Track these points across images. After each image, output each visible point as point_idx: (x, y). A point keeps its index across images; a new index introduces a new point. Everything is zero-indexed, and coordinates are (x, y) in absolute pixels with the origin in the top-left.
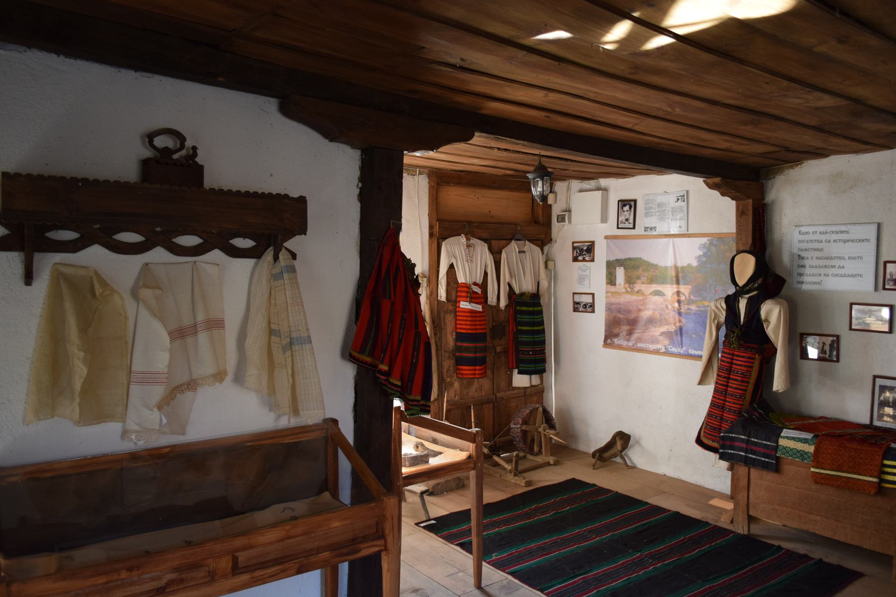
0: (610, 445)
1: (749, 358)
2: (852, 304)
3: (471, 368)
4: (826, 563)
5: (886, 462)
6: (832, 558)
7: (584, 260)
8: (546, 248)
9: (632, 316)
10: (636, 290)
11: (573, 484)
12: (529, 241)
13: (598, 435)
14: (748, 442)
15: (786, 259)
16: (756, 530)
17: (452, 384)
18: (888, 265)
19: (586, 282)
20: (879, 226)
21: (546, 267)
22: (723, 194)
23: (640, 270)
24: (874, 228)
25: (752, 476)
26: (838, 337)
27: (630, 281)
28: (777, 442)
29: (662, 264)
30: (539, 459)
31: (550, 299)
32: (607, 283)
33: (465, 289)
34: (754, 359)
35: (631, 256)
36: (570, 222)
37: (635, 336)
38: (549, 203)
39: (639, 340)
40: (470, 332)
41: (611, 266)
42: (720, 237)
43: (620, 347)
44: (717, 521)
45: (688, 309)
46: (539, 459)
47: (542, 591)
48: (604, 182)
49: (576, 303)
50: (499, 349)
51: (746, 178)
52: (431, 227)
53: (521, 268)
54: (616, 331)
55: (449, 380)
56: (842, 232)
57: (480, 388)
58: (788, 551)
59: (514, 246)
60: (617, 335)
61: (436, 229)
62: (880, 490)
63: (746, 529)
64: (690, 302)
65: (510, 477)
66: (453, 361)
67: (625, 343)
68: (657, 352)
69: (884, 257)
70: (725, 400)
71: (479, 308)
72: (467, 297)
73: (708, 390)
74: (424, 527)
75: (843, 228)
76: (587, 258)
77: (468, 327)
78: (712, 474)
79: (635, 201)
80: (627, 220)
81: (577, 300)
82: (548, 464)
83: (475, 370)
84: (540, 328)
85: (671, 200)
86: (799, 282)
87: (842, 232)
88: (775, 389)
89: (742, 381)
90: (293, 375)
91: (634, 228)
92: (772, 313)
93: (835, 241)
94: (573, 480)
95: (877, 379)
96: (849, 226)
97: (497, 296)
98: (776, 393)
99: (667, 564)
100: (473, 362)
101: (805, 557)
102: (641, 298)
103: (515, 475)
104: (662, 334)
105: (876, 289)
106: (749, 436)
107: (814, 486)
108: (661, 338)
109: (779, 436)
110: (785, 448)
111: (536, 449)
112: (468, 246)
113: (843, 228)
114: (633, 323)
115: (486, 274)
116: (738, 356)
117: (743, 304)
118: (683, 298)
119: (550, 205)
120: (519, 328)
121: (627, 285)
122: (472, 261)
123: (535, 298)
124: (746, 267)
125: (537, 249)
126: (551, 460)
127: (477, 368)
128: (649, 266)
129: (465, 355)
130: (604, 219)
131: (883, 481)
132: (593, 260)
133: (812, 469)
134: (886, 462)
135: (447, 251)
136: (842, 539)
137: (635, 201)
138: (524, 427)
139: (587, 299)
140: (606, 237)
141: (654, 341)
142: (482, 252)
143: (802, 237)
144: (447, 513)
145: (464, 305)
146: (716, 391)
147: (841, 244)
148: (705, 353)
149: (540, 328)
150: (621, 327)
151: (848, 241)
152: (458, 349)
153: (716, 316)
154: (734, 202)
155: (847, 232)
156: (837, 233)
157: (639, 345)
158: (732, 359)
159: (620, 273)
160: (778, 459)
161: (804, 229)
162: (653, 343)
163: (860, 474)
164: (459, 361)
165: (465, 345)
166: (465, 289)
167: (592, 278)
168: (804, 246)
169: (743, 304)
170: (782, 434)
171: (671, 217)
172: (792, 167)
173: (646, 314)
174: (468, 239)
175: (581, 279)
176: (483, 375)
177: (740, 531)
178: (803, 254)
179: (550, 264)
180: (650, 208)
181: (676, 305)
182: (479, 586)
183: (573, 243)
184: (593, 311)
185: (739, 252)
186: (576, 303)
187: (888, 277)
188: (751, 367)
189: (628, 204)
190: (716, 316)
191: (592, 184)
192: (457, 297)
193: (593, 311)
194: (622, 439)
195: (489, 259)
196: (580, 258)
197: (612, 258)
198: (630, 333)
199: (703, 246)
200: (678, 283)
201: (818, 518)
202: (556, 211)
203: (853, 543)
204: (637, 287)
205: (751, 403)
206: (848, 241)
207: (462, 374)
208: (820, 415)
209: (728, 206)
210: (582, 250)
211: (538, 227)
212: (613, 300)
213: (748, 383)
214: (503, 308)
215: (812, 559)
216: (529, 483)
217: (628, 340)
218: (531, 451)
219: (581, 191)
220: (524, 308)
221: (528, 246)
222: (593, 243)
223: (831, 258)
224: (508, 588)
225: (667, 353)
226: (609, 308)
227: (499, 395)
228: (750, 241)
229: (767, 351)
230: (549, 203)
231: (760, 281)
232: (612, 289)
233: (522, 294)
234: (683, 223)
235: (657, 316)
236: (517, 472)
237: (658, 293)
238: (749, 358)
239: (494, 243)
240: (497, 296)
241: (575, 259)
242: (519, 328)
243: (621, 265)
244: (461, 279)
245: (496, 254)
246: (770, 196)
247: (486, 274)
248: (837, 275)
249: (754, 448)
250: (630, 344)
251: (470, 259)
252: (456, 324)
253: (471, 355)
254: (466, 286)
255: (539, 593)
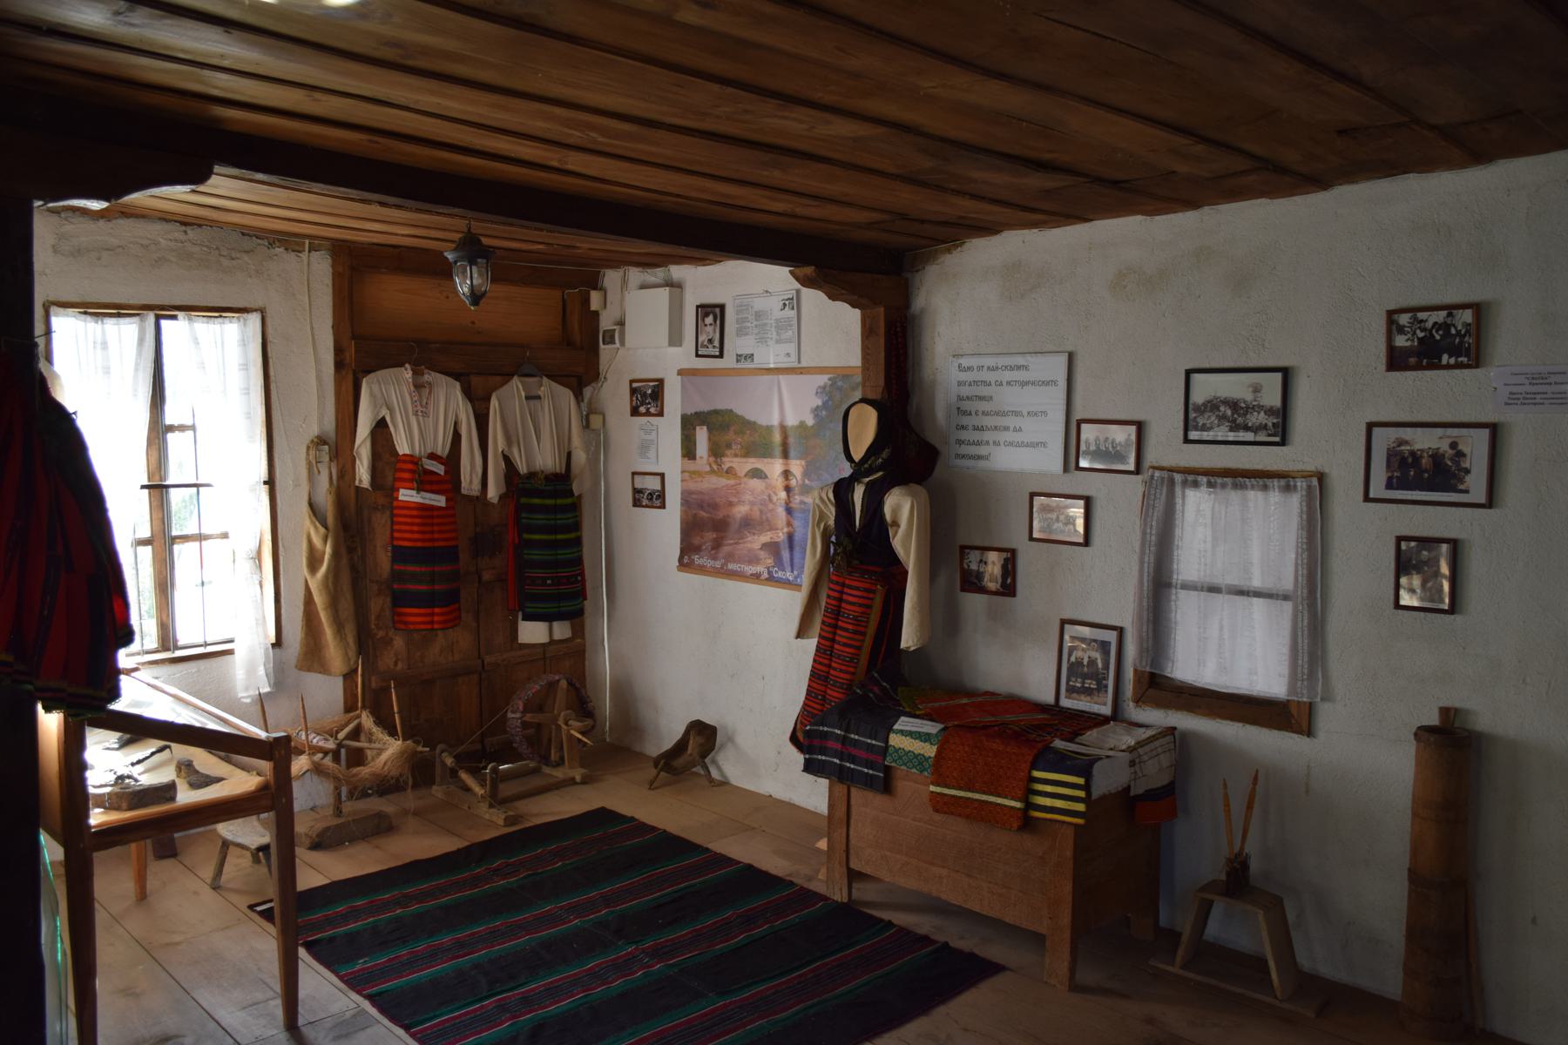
0: (681, 746)
1: (866, 590)
2: (1032, 495)
3: (422, 611)
4: (959, 952)
5: (1037, 774)
6: (962, 939)
7: (648, 414)
8: (588, 392)
9: (720, 515)
10: (725, 467)
11: (603, 816)
12: (548, 377)
13: (669, 729)
14: (844, 740)
15: (940, 415)
16: (863, 892)
17: (388, 642)
18: (1084, 426)
19: (652, 453)
20: (1071, 357)
21: (586, 425)
22: (832, 297)
23: (731, 433)
24: (1064, 359)
25: (853, 802)
26: (1013, 552)
27: (716, 452)
28: (886, 741)
29: (762, 421)
30: (559, 774)
31: (597, 484)
32: (684, 456)
33: (410, 466)
34: (874, 592)
35: (719, 407)
36: (623, 343)
37: (726, 549)
38: (593, 308)
39: (730, 557)
40: (419, 544)
41: (689, 423)
42: (840, 375)
43: (702, 570)
44: (810, 879)
45: (802, 502)
46: (559, 774)
47: (407, 1028)
48: (677, 271)
49: (637, 491)
50: (486, 576)
51: (876, 269)
52: (339, 351)
53: (533, 427)
54: (696, 541)
55: (381, 634)
56: (1019, 368)
57: (450, 646)
58: (901, 929)
59: (516, 387)
60: (697, 549)
61: (350, 354)
62: (1026, 822)
63: (845, 894)
64: (806, 490)
65: (485, 811)
66: (389, 600)
67: (709, 563)
68: (756, 578)
69: (1078, 414)
70: (829, 666)
71: (440, 501)
72: (411, 480)
73: (811, 644)
74: (261, 913)
75: (1020, 360)
76: (652, 410)
77: (416, 536)
78: (814, 794)
79: (722, 307)
80: (710, 341)
81: (638, 486)
82: (572, 782)
83: (433, 614)
84: (572, 535)
85: (774, 304)
86: (958, 456)
87: (1019, 368)
88: (903, 645)
89: (855, 632)
90: (1214, 589)
91: (721, 356)
92: (900, 506)
93: (1009, 383)
94: (603, 809)
95: (1067, 627)
96: (1029, 357)
97: (480, 477)
98: (906, 651)
99: (673, 965)
100: (428, 600)
101: (926, 940)
102: (732, 482)
103: (491, 806)
104: (765, 546)
105: (1066, 469)
106: (847, 731)
107: (938, 817)
108: (762, 554)
109: (890, 729)
110: (897, 750)
111: (554, 756)
112: (418, 386)
113: (1020, 360)
114: (721, 526)
115: (457, 437)
116: (850, 587)
117: (859, 493)
118: (793, 483)
119: (596, 314)
120: (526, 536)
121: (712, 459)
122: (425, 414)
123: (560, 482)
124: (865, 428)
125: (566, 395)
126: (578, 774)
127: (437, 610)
128: (748, 425)
129: (412, 587)
130: (675, 339)
131: (1030, 806)
132: (661, 414)
133: (932, 788)
134: (1037, 774)
135: (372, 395)
136: (977, 909)
137: (722, 307)
138: (528, 717)
139: (652, 484)
140: (681, 372)
141: (754, 560)
142: (450, 400)
143: (963, 376)
144: (327, 881)
145: (407, 495)
146: (819, 650)
147: (1017, 389)
148: (806, 580)
149: (572, 535)
150: (707, 535)
151: (1027, 383)
152: (396, 576)
153: (822, 516)
154: (857, 312)
155: (1026, 368)
156: (1012, 368)
157: (731, 566)
158: (842, 593)
159: (702, 435)
160: (888, 770)
161: (965, 362)
162: (750, 562)
163: (999, 795)
164: (399, 600)
165: (412, 568)
166: (410, 466)
167: (659, 448)
168: (966, 391)
169: (859, 493)
170: (896, 727)
171: (774, 335)
172: (949, 251)
173: (740, 511)
174: (415, 373)
175: (644, 448)
176: (453, 622)
177: (837, 897)
178: (966, 405)
179: (596, 421)
180: (744, 320)
181: (783, 495)
182: (291, 1024)
183: (631, 382)
184: (663, 506)
185: (863, 400)
186: (637, 491)
187: (1083, 447)
188: (870, 607)
189: (713, 312)
190: (822, 516)
191: (658, 274)
192: (395, 480)
193: (663, 506)
194: (703, 736)
195: (464, 413)
196: (642, 409)
197: (690, 411)
198: (717, 545)
199: (822, 390)
200: (785, 455)
201: (944, 872)
202: (606, 323)
203: (991, 914)
204: (728, 462)
205: (868, 671)
206: (1027, 383)
207: (406, 623)
208: (991, 688)
209: (849, 318)
210: (644, 395)
211: (575, 355)
212: (692, 486)
213: (864, 634)
214: (495, 501)
215: (933, 942)
216: (510, 821)
217: (715, 559)
218: (545, 759)
219: (643, 287)
220: (536, 501)
221: (546, 387)
222: (661, 381)
223: (1004, 414)
224: (347, 1027)
225: (772, 580)
226: (687, 500)
227: (488, 659)
228: (882, 382)
229: (894, 575)
230: (593, 308)
231: (885, 454)
232: (691, 465)
233: (532, 475)
234: (791, 348)
235: (756, 514)
236: (496, 800)
237: (757, 474)
238: (866, 590)
239: (476, 380)
240: (480, 477)
241: (635, 412)
242: (526, 536)
243: (702, 424)
244: (403, 448)
245: (479, 404)
246: (919, 302)
247: (457, 437)
248: (1011, 444)
249: (855, 752)
250: (718, 564)
251: (422, 410)
252: (392, 531)
253: (423, 588)
254: (412, 460)
255: (401, 1032)
